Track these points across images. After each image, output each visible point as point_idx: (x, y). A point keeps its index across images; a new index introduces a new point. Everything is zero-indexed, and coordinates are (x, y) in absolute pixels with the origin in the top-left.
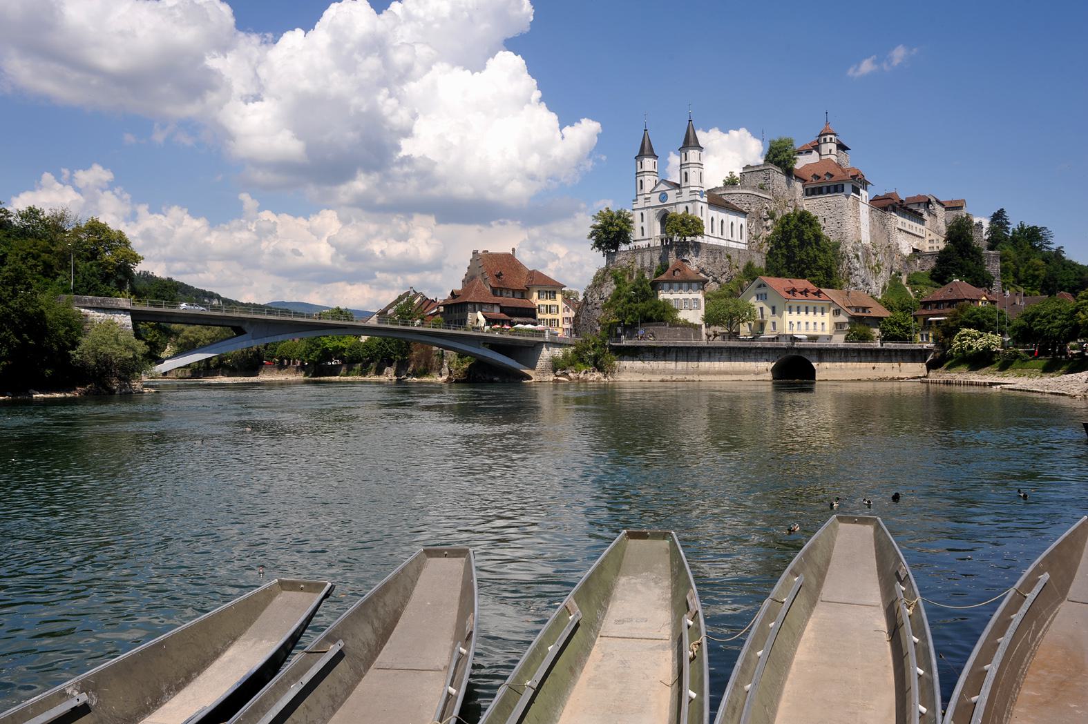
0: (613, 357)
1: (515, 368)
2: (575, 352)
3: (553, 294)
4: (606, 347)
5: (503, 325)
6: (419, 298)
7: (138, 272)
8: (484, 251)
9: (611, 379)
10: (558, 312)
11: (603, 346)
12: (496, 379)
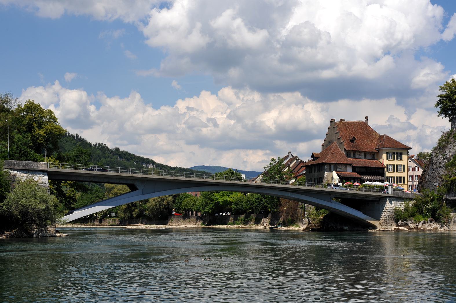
0: (449, 209)
1: (362, 219)
2: (415, 205)
3: (399, 155)
4: (443, 200)
5: (354, 182)
6: (295, 161)
7: (95, 144)
8: (341, 120)
9: (447, 229)
10: (404, 171)
11: (440, 199)
12: (346, 228)
